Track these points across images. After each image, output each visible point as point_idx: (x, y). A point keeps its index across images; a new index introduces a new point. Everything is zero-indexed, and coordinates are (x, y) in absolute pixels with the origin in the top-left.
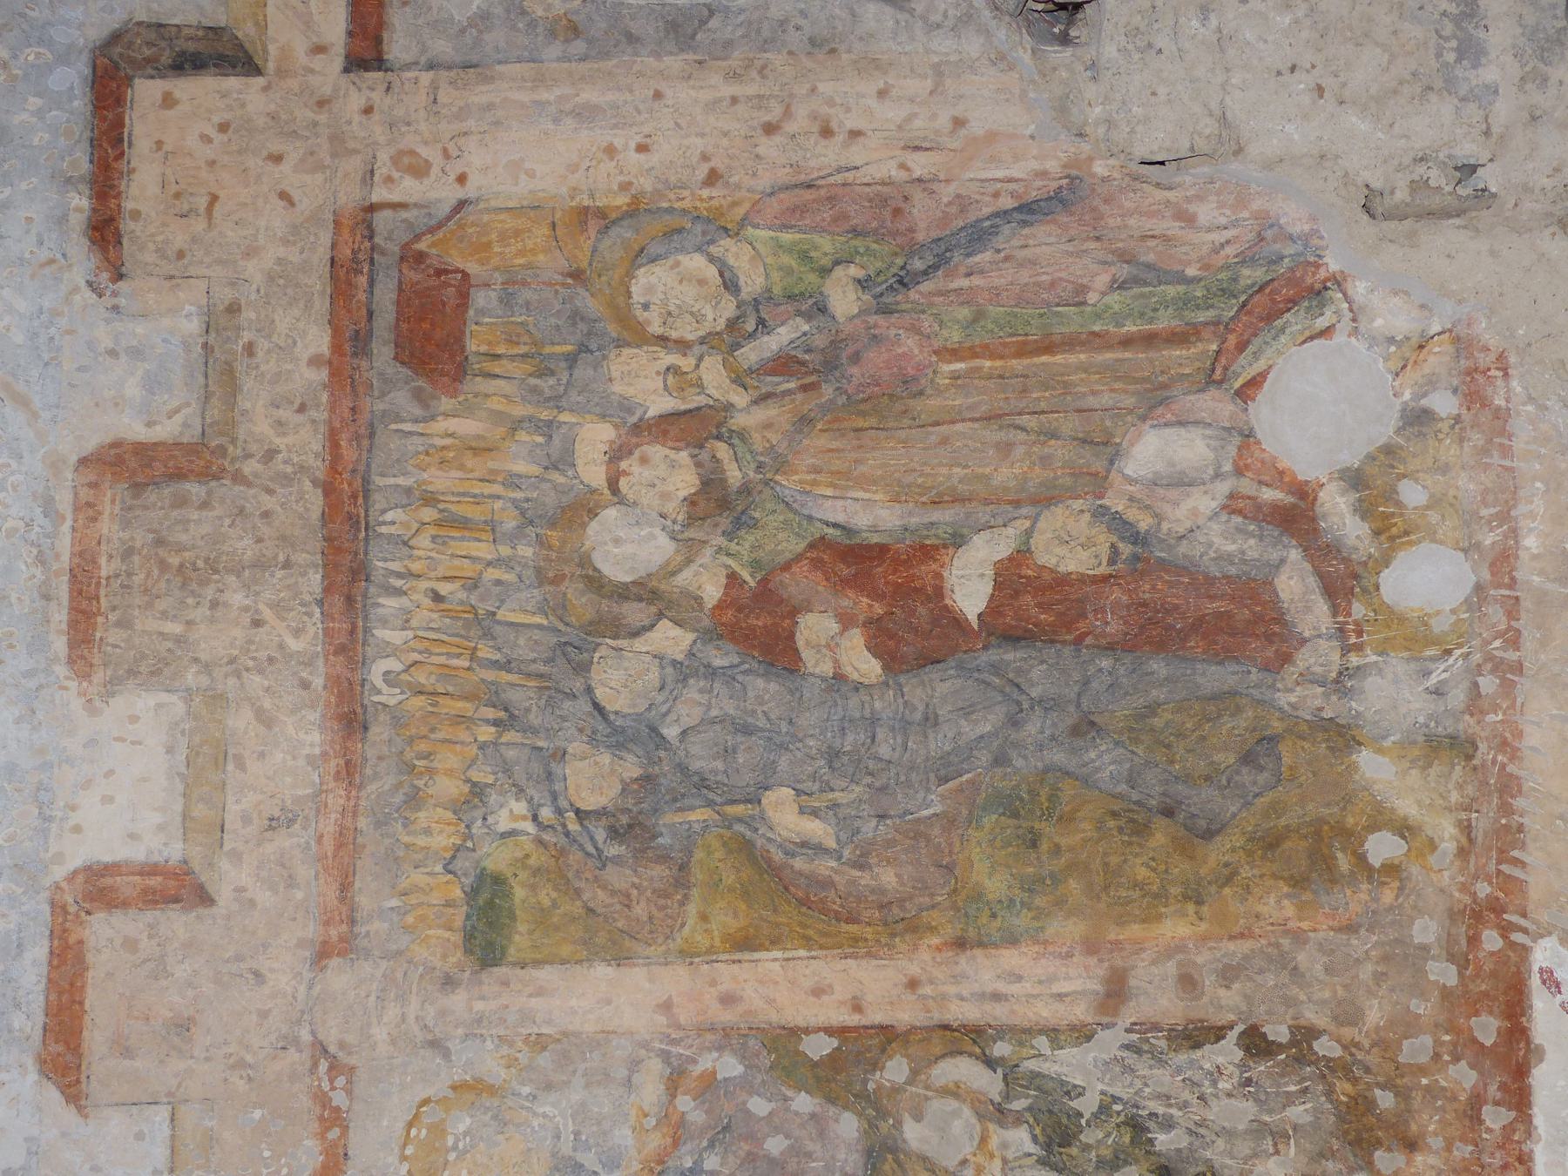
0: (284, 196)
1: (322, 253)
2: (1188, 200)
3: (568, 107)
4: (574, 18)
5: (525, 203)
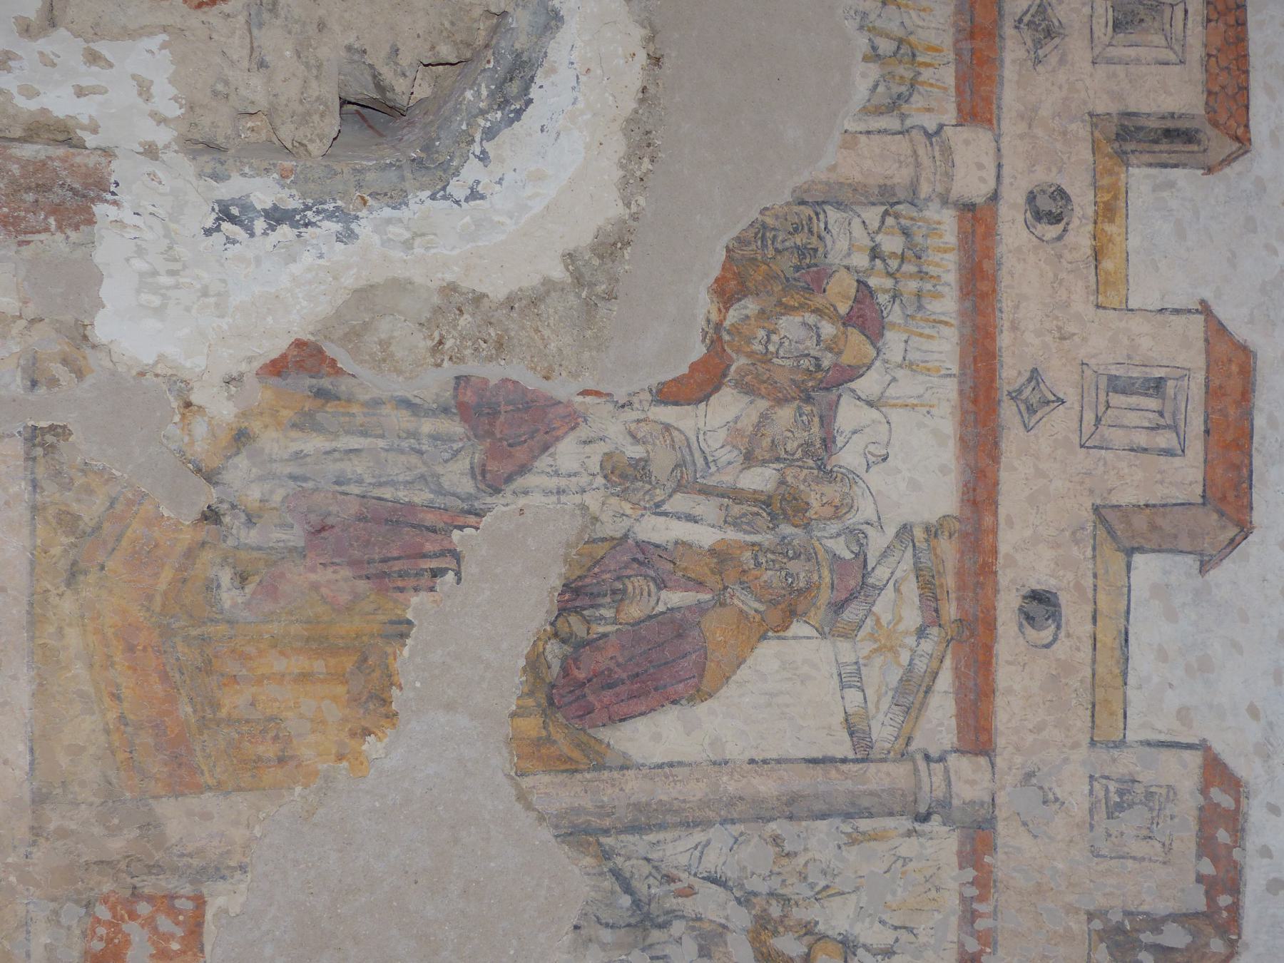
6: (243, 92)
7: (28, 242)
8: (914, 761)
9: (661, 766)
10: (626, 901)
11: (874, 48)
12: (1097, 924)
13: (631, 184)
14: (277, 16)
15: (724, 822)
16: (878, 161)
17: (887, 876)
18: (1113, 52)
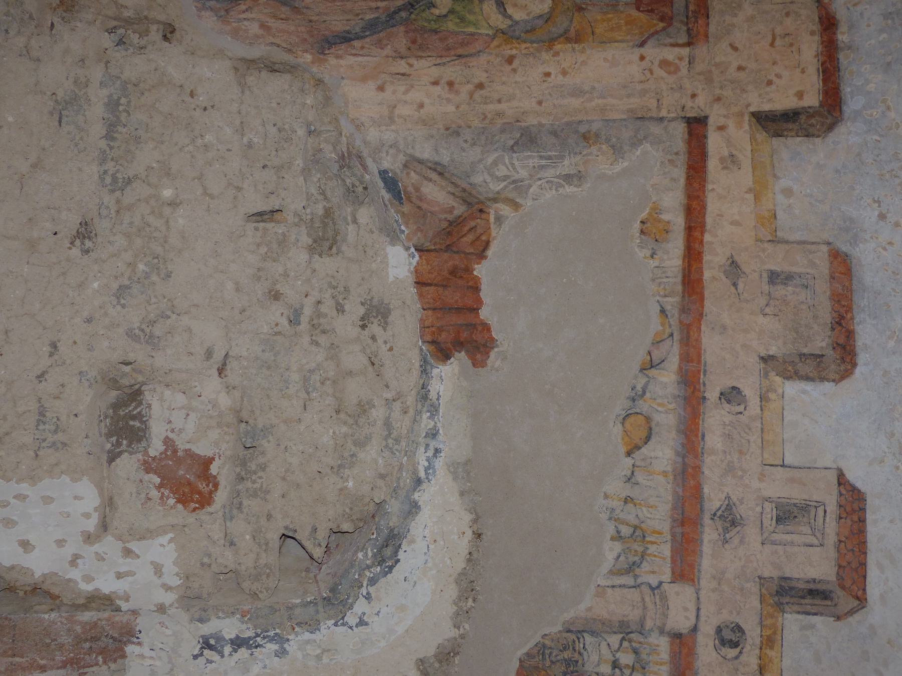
0: (736, 49)
1: (714, 20)
2: (263, 36)
3: (587, 96)
4: (586, 144)
5: (608, 45)
6: (220, 560)
7: (86, 673)
11: (618, 532)
13: (460, 615)
14: (242, 512)
16: (621, 605)
18: (775, 537)
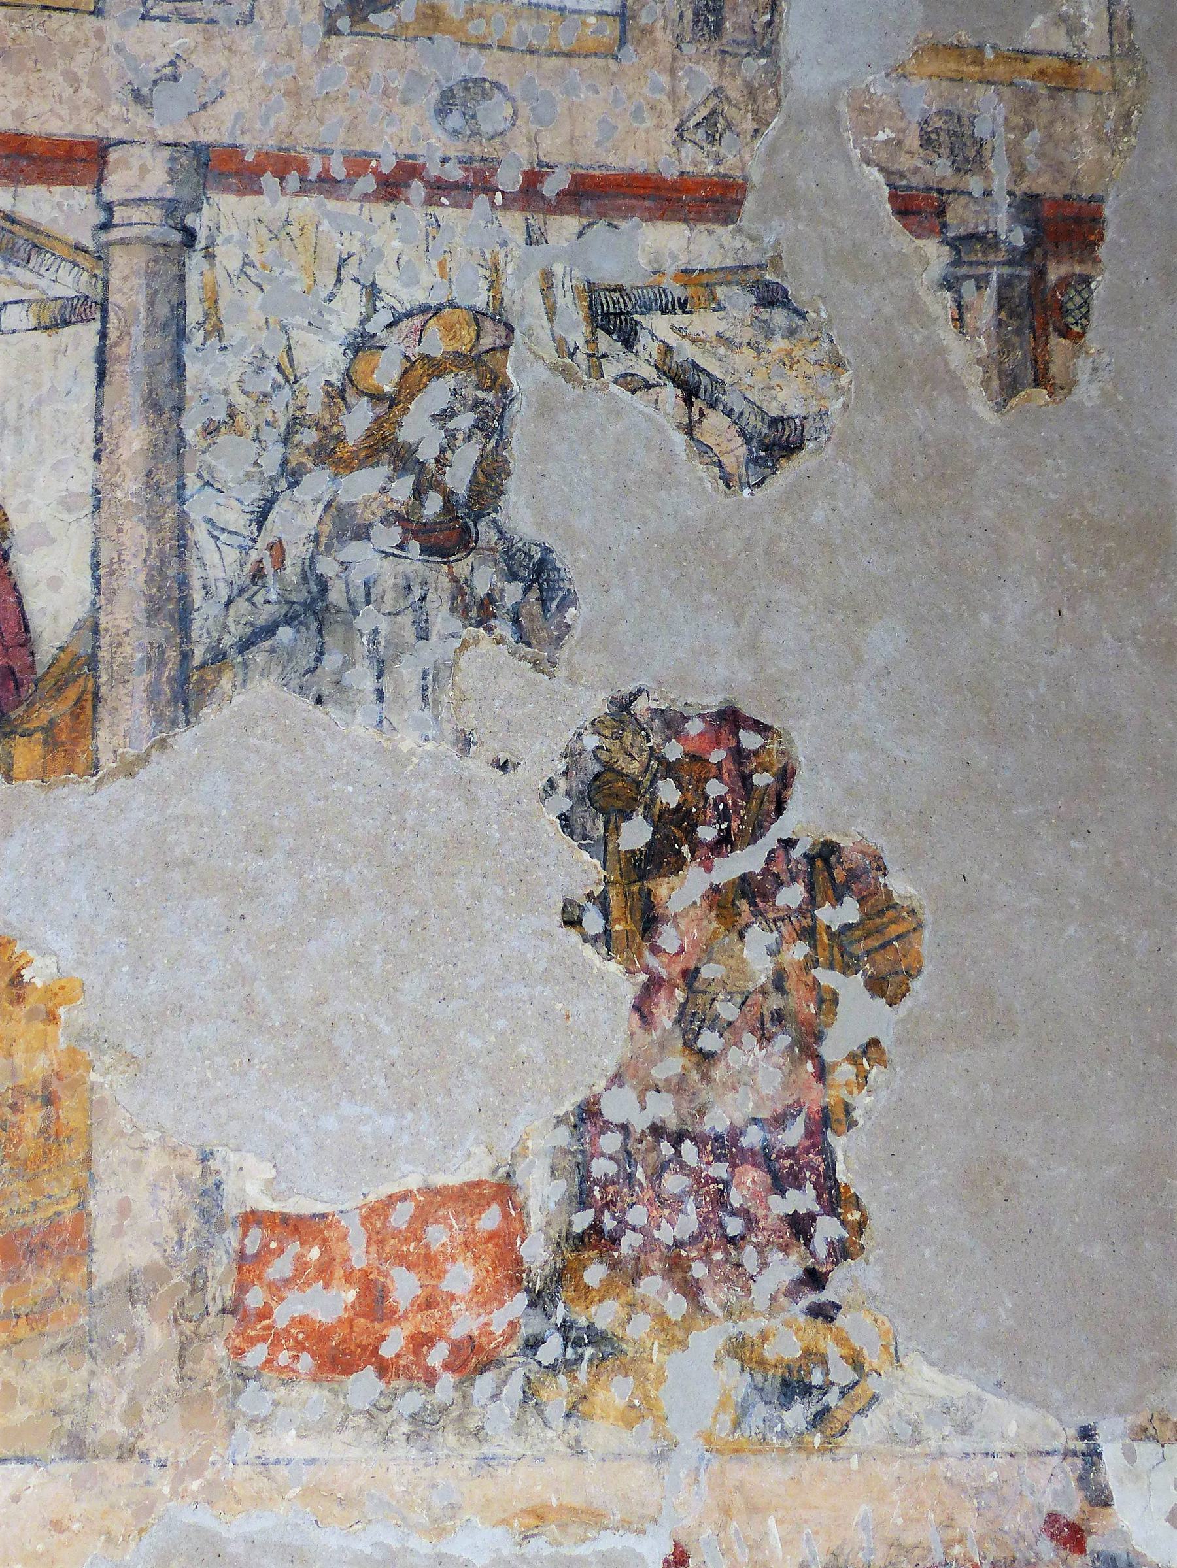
8: (108, 245)
9: (97, 580)
10: (285, 634)
12: (344, 23)
15: (181, 499)
17: (266, 288)
